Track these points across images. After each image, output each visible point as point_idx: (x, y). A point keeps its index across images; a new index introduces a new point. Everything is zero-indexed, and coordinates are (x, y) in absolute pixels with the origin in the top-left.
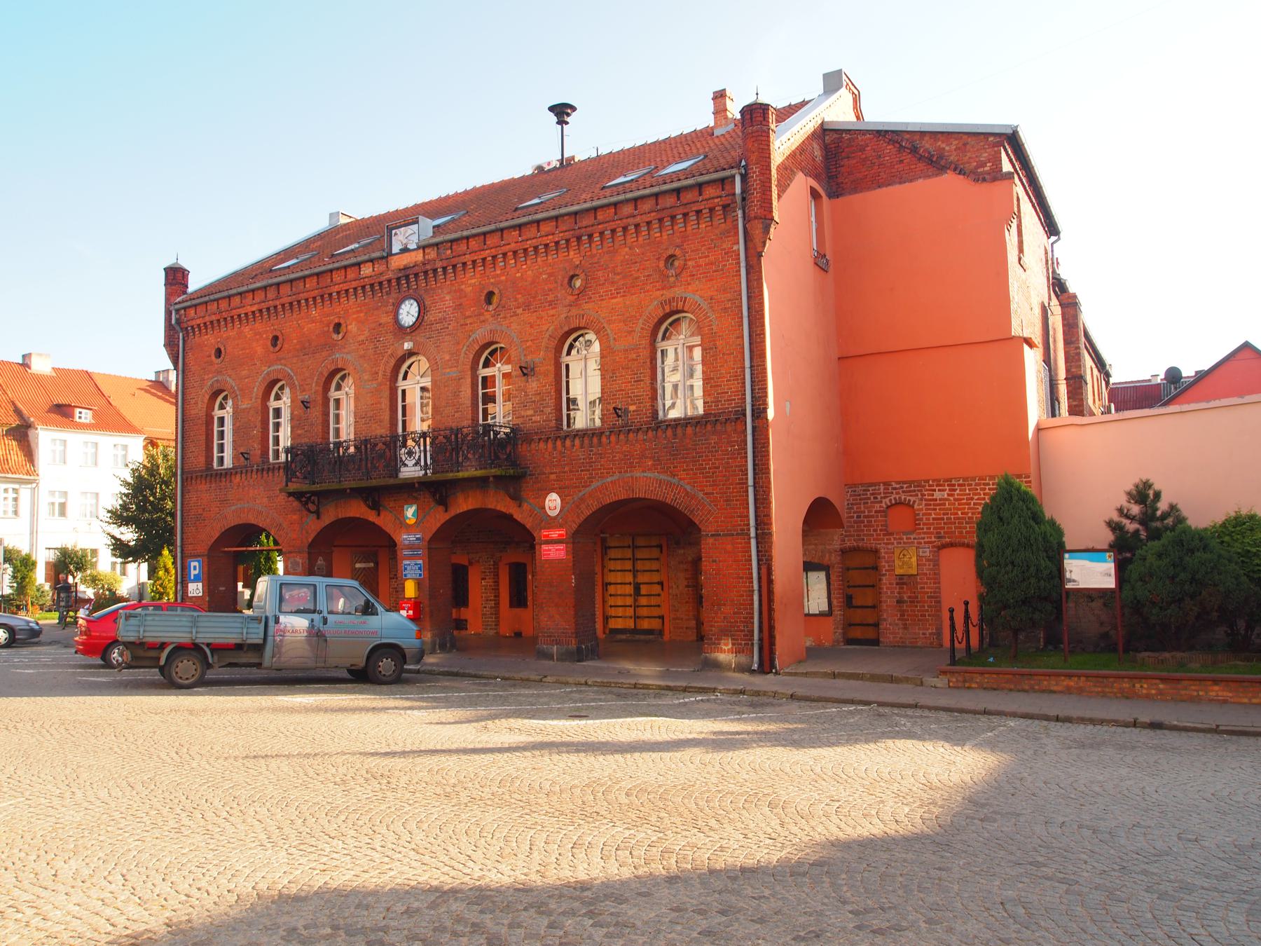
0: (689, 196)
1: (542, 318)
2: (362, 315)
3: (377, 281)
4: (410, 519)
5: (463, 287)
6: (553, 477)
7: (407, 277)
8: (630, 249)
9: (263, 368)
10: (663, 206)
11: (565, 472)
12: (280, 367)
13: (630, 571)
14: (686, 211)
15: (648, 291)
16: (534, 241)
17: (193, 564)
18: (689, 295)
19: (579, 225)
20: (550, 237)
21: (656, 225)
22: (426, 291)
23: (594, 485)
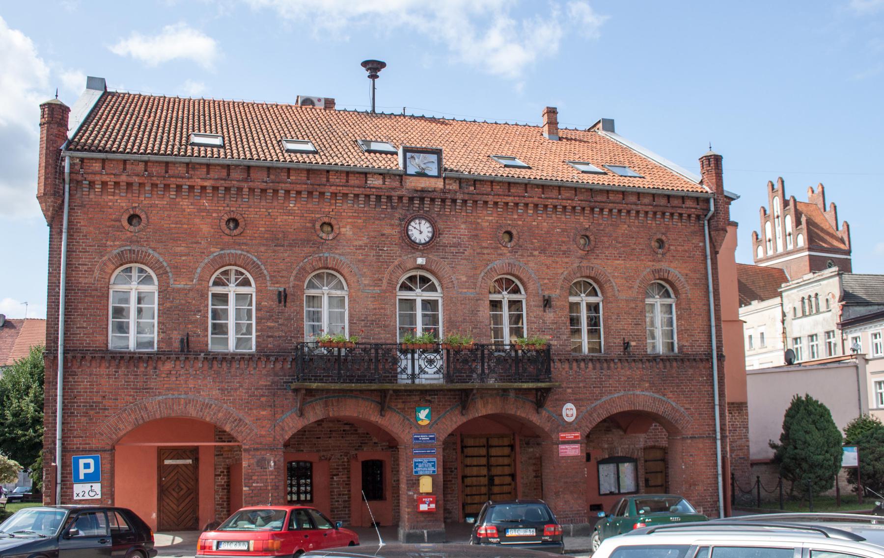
0: (675, 202)
1: (557, 262)
2: (359, 221)
3: (387, 194)
4: (422, 420)
5: (479, 221)
6: (569, 391)
7: (422, 199)
8: (629, 226)
9: (212, 250)
10: (658, 203)
11: (580, 388)
12: (239, 252)
13: (485, 466)
14: (673, 211)
15: (643, 260)
16: (554, 201)
17: (82, 462)
18: (672, 270)
19: (595, 199)
20: (569, 202)
21: (650, 215)
22: (438, 215)
23: (604, 399)
